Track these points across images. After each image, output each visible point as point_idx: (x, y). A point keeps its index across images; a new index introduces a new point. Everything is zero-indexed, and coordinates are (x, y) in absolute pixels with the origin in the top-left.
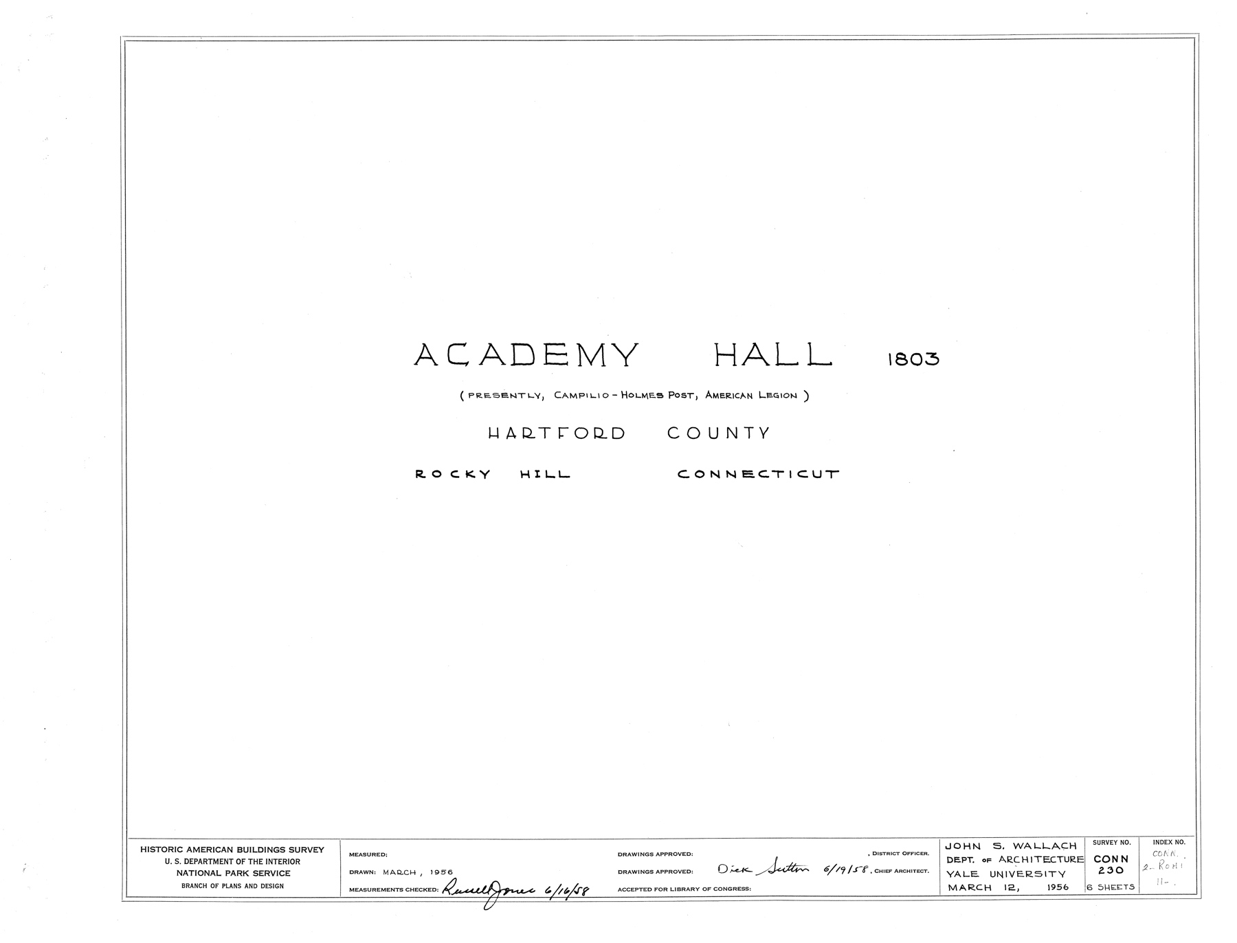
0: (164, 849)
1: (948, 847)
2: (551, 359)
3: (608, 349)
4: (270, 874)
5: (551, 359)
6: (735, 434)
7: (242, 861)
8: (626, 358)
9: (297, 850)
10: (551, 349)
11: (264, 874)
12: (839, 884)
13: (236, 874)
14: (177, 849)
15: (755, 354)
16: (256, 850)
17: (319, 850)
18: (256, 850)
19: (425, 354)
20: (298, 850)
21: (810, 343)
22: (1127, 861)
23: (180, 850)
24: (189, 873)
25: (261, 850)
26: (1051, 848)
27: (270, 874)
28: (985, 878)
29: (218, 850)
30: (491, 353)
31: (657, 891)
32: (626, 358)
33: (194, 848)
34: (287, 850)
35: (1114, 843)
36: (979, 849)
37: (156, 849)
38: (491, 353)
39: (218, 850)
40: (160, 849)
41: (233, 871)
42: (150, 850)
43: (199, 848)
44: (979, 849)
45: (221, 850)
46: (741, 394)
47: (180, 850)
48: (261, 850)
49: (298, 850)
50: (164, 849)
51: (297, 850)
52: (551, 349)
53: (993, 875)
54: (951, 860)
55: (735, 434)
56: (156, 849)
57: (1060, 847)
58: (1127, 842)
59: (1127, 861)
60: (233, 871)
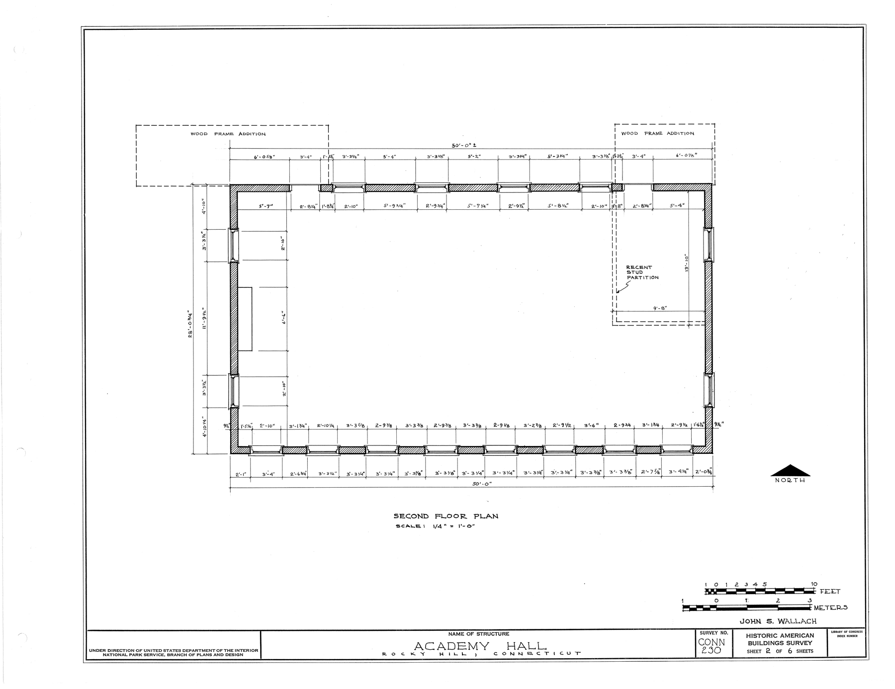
1: (742, 622)
6: (470, 646)
7: (193, 655)
9: (793, 643)
10: (460, 644)
11: (794, 636)
12: (147, 658)
13: (784, 636)
14: (424, 516)
15: (441, 646)
16: (762, 643)
17: (808, 643)
18: (762, 643)
19: (441, 646)
20: (755, 644)
22: (813, 637)
23: (775, 636)
25: (766, 643)
29: (803, 636)
31: (199, 656)
33: (811, 634)
35: (715, 633)
36: (497, 517)
37: (758, 636)
39: (803, 636)
42: (753, 636)
43: (789, 634)
44: (497, 517)
47: (775, 636)
48: (766, 643)
49: (755, 644)
51: (793, 643)
52: (460, 644)
55: (470, 646)
56: (758, 636)
58: (725, 633)
59: (813, 637)
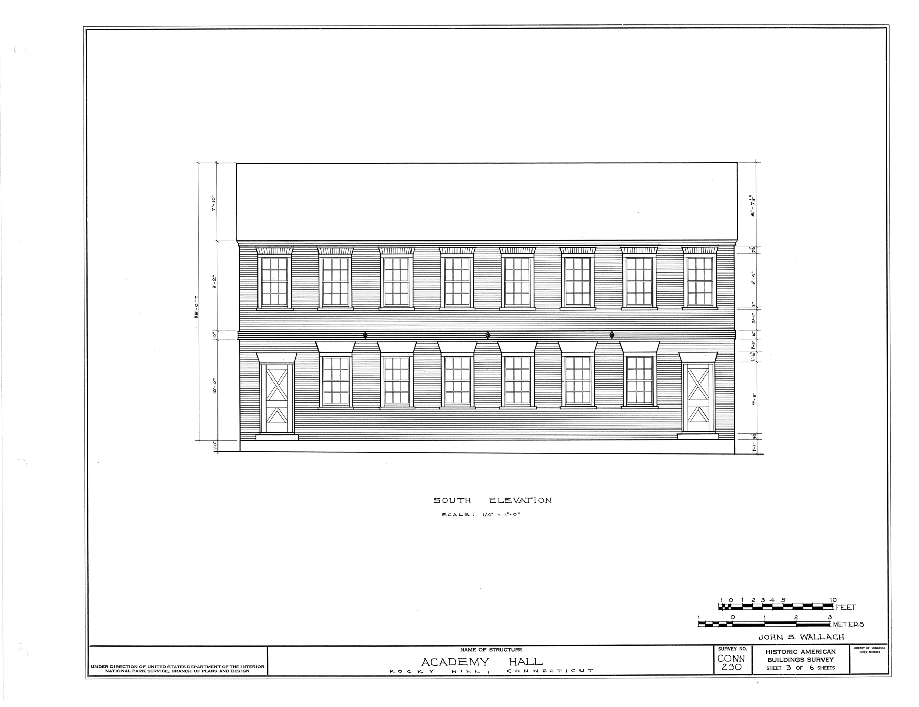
2: (461, 663)
3: (479, 660)
5: (461, 663)
6: (477, 662)
8: (485, 663)
10: (461, 660)
11: (815, 652)
13: (805, 652)
17: (829, 659)
18: (782, 659)
19: (521, 661)
20: (814, 660)
21: (535, 658)
23: (795, 652)
25: (786, 660)
26: (826, 638)
29: (825, 652)
30: (426, 662)
32: (485, 663)
37: (778, 652)
38: (443, 662)
39: (825, 652)
41: (829, 650)
42: (773, 652)
43: (810, 650)
45: (827, 652)
46: (827, 651)
47: (795, 652)
49: (814, 660)
50: (784, 652)
52: (461, 660)
56: (778, 652)
57: (832, 637)
60: (829, 650)
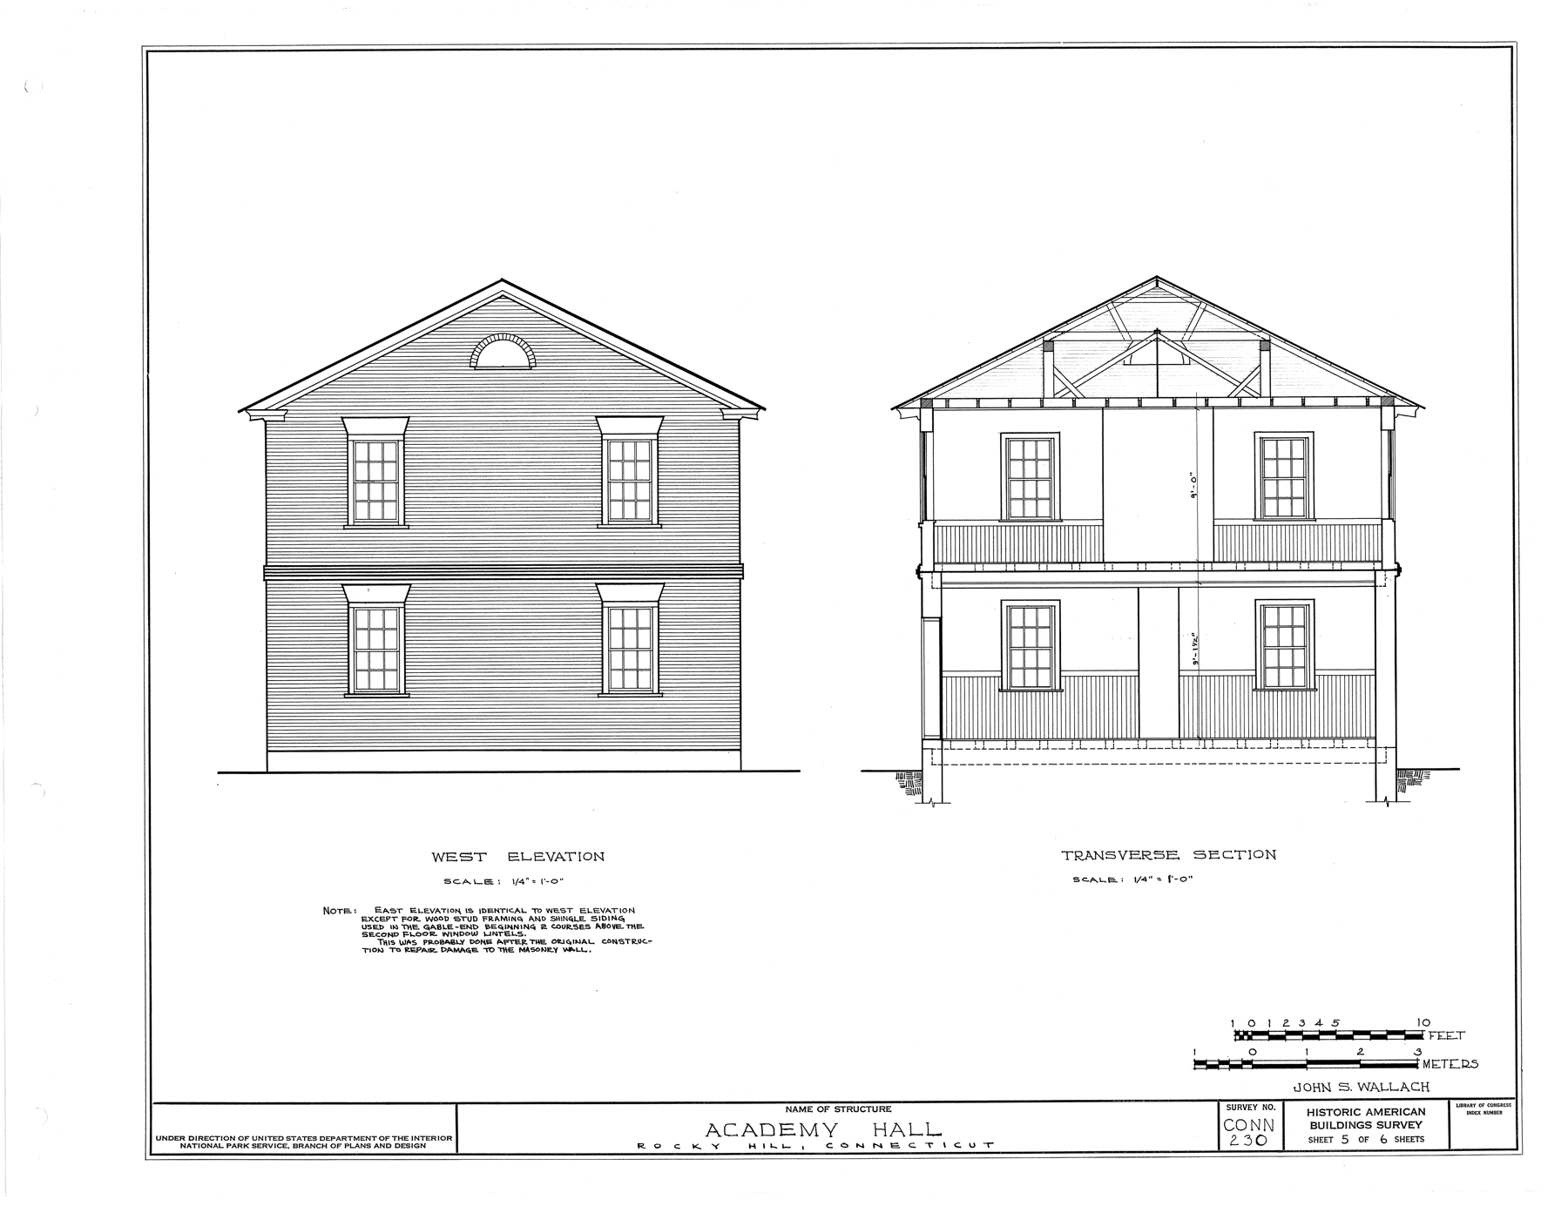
0: (1337, 1112)
2: (784, 1132)
4: (1400, 1126)
5: (784, 1132)
10: (784, 1127)
15: (713, 1129)
16: (1334, 1125)
17: (1415, 1125)
18: (1334, 1125)
20: (1321, 1126)
22: (1424, 1114)
23: (1357, 1112)
24: (193, 1146)
25: (1340, 1125)
27: (1400, 1126)
28: (548, 916)
29: (1407, 1112)
32: (831, 1133)
34: (1374, 1125)
38: (897, 1129)
39: (1407, 1112)
40: (1332, 1112)
42: (1319, 1113)
45: (1410, 1112)
47: (1357, 1112)
48: (1340, 1125)
49: (1321, 1126)
52: (784, 1127)
53: (1345, 1141)
54: (1314, 1126)
56: (1327, 1112)
59: (1424, 1114)
